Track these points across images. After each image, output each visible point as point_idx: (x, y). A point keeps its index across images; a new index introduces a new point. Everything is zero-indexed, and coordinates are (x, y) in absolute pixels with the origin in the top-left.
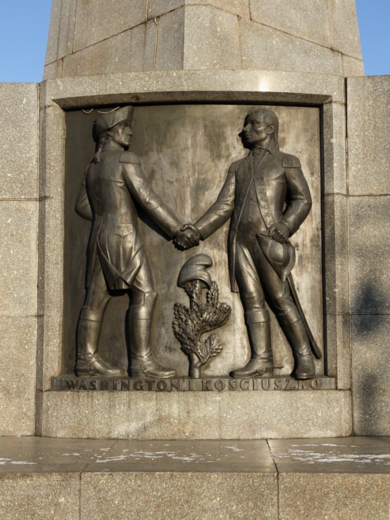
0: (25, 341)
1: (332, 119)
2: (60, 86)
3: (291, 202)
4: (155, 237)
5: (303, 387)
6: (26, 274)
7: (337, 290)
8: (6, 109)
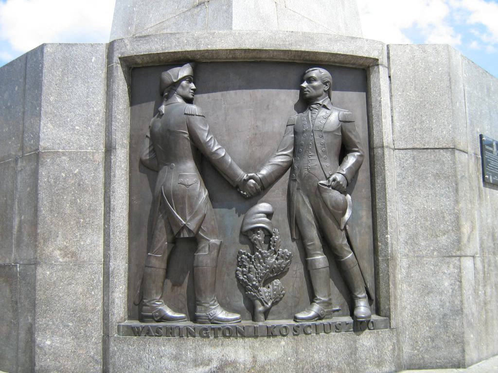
0: (91, 288)
1: (379, 80)
6: (92, 223)
7: (389, 236)
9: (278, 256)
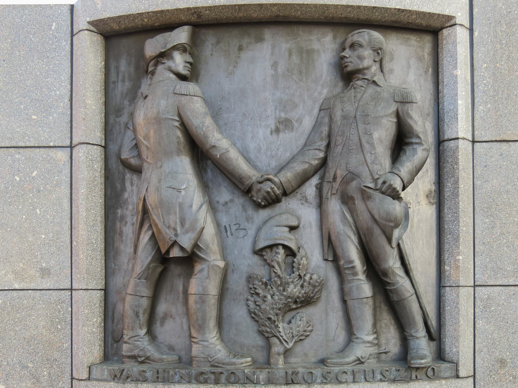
0: (57, 320)
1: (456, 46)
2: (98, 4)
3: (405, 148)
4: (224, 194)
5: (416, 377)
7: (461, 258)
8: (31, 36)
9: (304, 281)
